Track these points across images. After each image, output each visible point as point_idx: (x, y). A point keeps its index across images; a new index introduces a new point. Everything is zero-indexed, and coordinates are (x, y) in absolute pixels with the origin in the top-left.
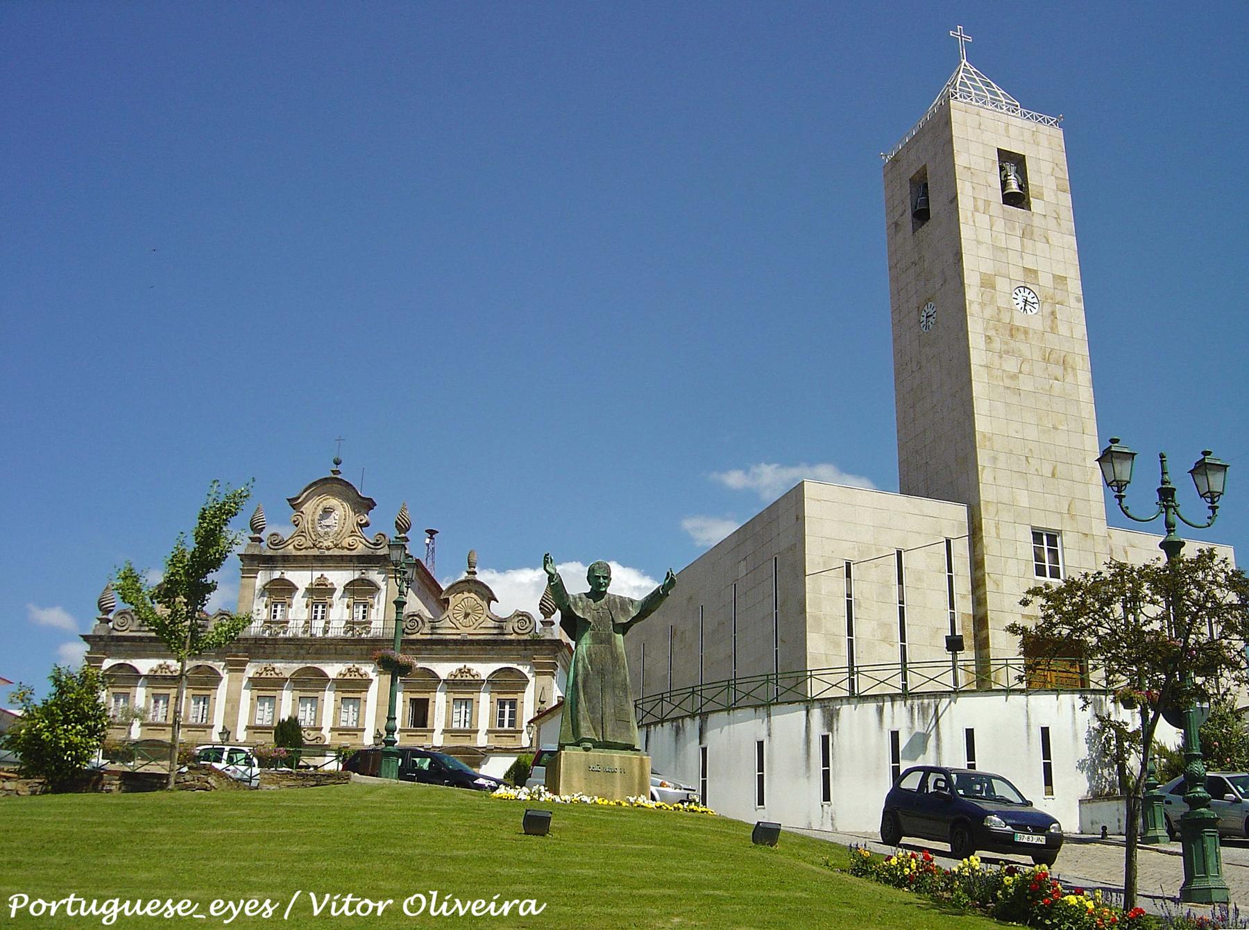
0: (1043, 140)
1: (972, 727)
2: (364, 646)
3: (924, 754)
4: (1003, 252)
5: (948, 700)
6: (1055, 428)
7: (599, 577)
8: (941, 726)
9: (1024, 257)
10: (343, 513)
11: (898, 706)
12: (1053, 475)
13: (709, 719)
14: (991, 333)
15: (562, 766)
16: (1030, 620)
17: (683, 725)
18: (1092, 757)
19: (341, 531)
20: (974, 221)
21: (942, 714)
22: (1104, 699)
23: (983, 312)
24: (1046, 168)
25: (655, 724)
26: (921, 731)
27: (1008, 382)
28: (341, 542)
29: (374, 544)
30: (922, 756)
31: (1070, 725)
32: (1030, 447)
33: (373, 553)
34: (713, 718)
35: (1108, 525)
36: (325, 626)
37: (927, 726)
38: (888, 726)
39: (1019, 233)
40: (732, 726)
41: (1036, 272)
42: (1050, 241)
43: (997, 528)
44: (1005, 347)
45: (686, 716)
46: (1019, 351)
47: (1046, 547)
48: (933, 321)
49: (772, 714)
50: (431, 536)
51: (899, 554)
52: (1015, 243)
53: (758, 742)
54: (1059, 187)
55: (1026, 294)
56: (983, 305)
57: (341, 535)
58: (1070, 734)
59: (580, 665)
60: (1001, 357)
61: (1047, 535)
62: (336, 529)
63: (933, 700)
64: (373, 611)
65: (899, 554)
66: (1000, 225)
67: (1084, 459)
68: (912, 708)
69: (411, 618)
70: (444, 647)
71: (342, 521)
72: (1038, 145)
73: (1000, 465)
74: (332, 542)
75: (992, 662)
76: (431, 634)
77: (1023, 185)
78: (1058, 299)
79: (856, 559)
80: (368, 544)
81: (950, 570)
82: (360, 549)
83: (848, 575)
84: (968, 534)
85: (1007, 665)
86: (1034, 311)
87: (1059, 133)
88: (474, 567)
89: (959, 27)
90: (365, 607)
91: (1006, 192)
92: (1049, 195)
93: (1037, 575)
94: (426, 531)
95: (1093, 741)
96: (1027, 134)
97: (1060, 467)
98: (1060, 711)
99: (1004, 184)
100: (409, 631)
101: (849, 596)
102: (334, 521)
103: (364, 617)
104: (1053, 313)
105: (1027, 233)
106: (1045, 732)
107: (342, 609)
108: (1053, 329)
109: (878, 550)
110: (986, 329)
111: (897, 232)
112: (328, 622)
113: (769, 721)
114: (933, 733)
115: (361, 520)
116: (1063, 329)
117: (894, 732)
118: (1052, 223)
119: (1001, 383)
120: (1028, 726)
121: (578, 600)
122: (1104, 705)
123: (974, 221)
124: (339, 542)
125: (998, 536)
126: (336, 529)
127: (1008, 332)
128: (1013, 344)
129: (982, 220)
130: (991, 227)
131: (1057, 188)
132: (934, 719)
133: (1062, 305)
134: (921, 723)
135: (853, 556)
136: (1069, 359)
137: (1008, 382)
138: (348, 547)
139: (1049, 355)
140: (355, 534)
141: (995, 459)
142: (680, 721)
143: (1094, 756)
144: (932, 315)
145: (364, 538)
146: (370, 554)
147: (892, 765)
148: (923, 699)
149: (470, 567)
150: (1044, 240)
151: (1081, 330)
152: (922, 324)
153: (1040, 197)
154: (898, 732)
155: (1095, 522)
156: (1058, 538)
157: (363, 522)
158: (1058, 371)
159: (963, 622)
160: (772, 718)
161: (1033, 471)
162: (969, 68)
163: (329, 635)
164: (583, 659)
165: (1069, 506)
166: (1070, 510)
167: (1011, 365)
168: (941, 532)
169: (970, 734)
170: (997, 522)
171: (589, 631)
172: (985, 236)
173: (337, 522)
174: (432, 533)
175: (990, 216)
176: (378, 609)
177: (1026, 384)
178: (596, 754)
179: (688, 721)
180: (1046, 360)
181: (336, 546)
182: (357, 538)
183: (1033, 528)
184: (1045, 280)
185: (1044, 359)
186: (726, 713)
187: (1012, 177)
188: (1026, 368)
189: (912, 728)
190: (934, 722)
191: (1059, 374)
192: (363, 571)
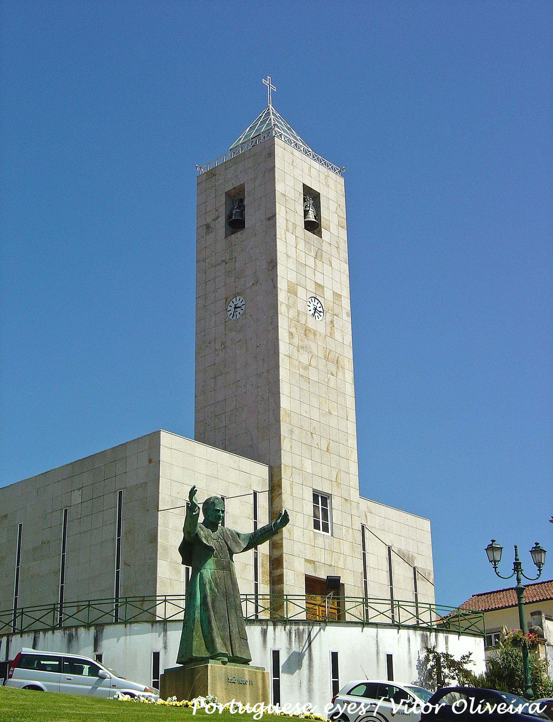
0: (331, 183)
1: (391, 654)
3: (300, 669)
4: (303, 267)
5: (318, 628)
7: (219, 510)
8: (313, 649)
11: (279, 629)
12: (328, 450)
13: (105, 630)
14: (293, 330)
15: (209, 677)
16: (310, 564)
17: (76, 634)
18: (421, 680)
20: (286, 238)
21: (314, 638)
22: (429, 635)
24: (333, 207)
25: (45, 631)
26: (297, 651)
27: (302, 372)
30: (297, 671)
31: (407, 654)
34: (108, 630)
35: (360, 496)
37: (301, 648)
38: (271, 646)
39: (313, 254)
40: (128, 637)
41: (323, 287)
42: (332, 264)
45: (81, 626)
48: (241, 312)
49: (168, 630)
52: (311, 262)
53: (153, 653)
55: (315, 304)
56: (288, 306)
58: (407, 661)
59: (208, 587)
60: (298, 351)
61: (321, 497)
63: (307, 627)
68: (290, 632)
75: (346, 599)
77: (318, 215)
84: (268, 490)
86: (321, 318)
87: (342, 181)
89: (268, 77)
92: (333, 228)
93: (314, 528)
95: (421, 667)
96: (322, 177)
98: (400, 643)
99: (306, 213)
104: (332, 322)
105: (318, 256)
106: (389, 658)
108: (332, 335)
110: (289, 327)
111: (207, 233)
113: (165, 635)
114: (307, 653)
116: (338, 336)
117: (389, 655)
118: (334, 251)
120: (378, 653)
122: (429, 640)
123: (286, 238)
125: (292, 493)
127: (303, 332)
132: (307, 642)
134: (297, 645)
136: (340, 359)
137: (302, 372)
139: (329, 354)
142: (74, 630)
143: (422, 679)
144: (240, 307)
147: (332, 680)
148: (299, 625)
150: (329, 263)
151: (349, 339)
152: (230, 313)
153: (328, 229)
154: (279, 651)
156: (328, 500)
158: (333, 369)
159: (263, 561)
160: (168, 632)
162: (275, 113)
164: (210, 584)
165: (337, 476)
167: (304, 358)
169: (335, 656)
171: (212, 558)
172: (292, 252)
178: (230, 666)
179: (82, 631)
180: (326, 358)
183: (314, 490)
184: (328, 295)
186: (124, 625)
188: (313, 363)
189: (290, 649)
190: (307, 645)
191: (334, 370)
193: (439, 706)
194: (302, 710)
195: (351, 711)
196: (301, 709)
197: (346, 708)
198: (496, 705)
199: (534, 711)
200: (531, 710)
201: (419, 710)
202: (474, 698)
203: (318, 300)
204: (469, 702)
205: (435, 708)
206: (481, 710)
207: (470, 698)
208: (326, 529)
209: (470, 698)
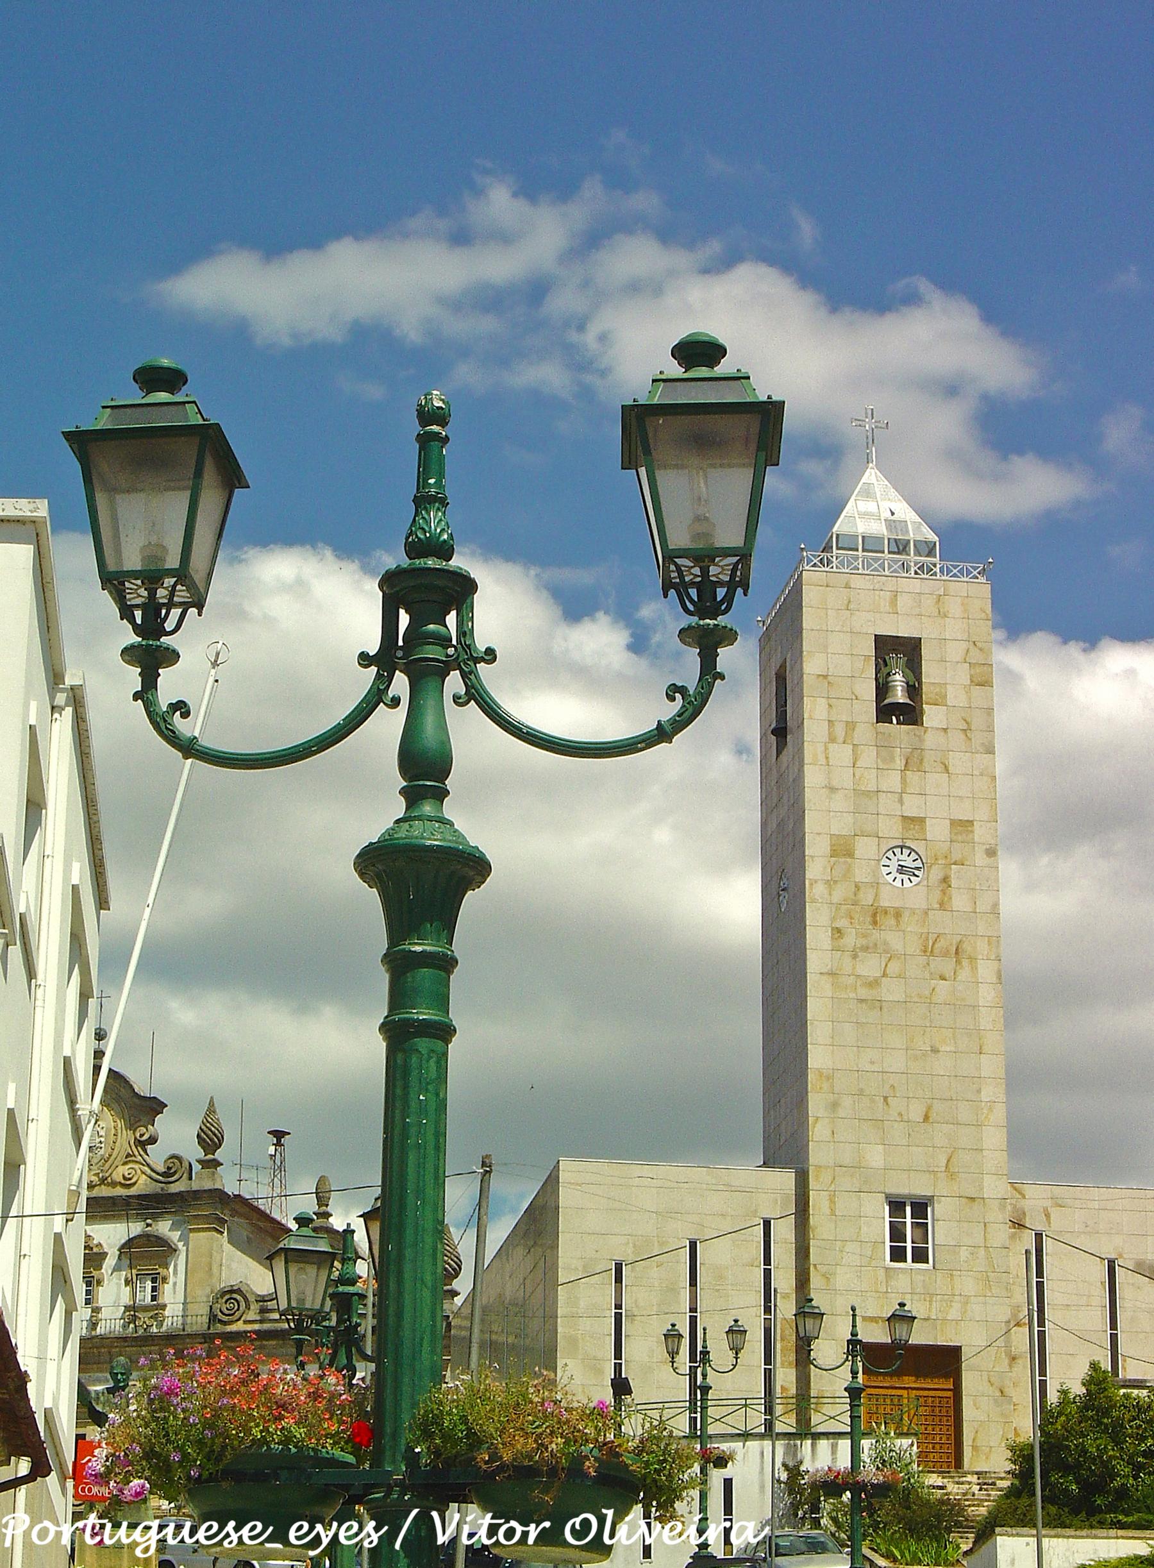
2: (153, 1348)
6: (935, 1050)
9: (905, 800)
10: (113, 1124)
12: (926, 1118)
14: (842, 923)
19: (110, 1156)
23: (830, 895)
27: (863, 993)
28: (111, 1174)
29: (163, 1174)
32: (891, 1082)
33: (162, 1189)
36: (92, 1316)
39: (899, 763)
41: (922, 820)
42: (951, 769)
43: (832, 1201)
44: (862, 942)
46: (886, 943)
47: (909, 1220)
50: (279, 1141)
51: (693, 1245)
52: (893, 781)
54: (974, 679)
56: (831, 883)
57: (110, 1162)
60: (855, 957)
61: (912, 1204)
62: (102, 1152)
64: (168, 1288)
65: (693, 1245)
66: (868, 757)
67: (979, 1091)
69: (227, 1297)
70: (281, 1342)
71: (112, 1138)
72: (946, 616)
73: (841, 1113)
74: (97, 1175)
76: (261, 1321)
77: (914, 690)
78: (956, 856)
79: (630, 1259)
80: (154, 1175)
81: (767, 1261)
82: (142, 1185)
83: (619, 1279)
84: (794, 1211)
85: (746, 1405)
88: (327, 1205)
90: (154, 1280)
91: (886, 702)
94: (268, 1133)
96: (929, 602)
97: (938, 1106)
99: (883, 689)
100: (225, 1318)
101: (618, 1306)
102: (98, 1140)
103: (154, 1298)
104: (945, 880)
107: (119, 1285)
109: (661, 1244)
110: (833, 919)
112: (96, 1310)
115: (142, 1135)
118: (957, 739)
119: (852, 995)
121: (100, 1395)
124: (107, 1175)
125: (833, 1212)
126: (102, 1152)
127: (869, 919)
128: (876, 935)
129: (842, 754)
130: (854, 764)
131: (972, 681)
133: (963, 865)
135: (625, 1253)
138: (123, 1182)
140: (133, 1158)
141: (835, 1105)
145: (148, 1165)
146: (159, 1191)
149: (320, 1205)
150: (940, 768)
154: (731, 1479)
155: (988, 1180)
157: (145, 1138)
158: (946, 965)
161: (894, 1114)
163: (99, 1331)
165: (948, 1161)
166: (950, 1166)
167: (870, 967)
168: (756, 1211)
170: (833, 1193)
173: (102, 1139)
174: (279, 1135)
175: (854, 745)
176: (175, 1284)
177: (892, 991)
181: (103, 1181)
182: (137, 1166)
184: (938, 831)
185: (925, 951)
187: (897, 677)
192: (149, 1221)
193: (716, 1529)
194: (241, 1535)
195: (348, 1538)
196: (239, 1534)
197: (660, 1534)
198: (335, 1524)
199: (194, 1539)
200: (89, 1536)
201: (493, 1537)
202: (613, 1510)
203: (909, 848)
204: (602, 1520)
205: (528, 1531)
206: (628, 1538)
207: (604, 1511)
208: (920, 1256)
209: (604, 1511)
